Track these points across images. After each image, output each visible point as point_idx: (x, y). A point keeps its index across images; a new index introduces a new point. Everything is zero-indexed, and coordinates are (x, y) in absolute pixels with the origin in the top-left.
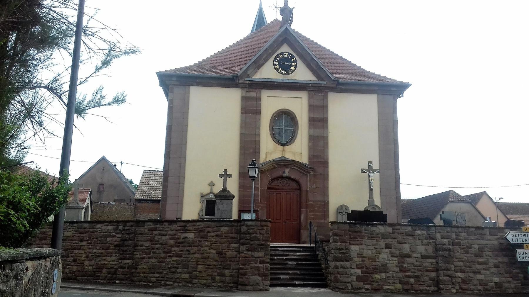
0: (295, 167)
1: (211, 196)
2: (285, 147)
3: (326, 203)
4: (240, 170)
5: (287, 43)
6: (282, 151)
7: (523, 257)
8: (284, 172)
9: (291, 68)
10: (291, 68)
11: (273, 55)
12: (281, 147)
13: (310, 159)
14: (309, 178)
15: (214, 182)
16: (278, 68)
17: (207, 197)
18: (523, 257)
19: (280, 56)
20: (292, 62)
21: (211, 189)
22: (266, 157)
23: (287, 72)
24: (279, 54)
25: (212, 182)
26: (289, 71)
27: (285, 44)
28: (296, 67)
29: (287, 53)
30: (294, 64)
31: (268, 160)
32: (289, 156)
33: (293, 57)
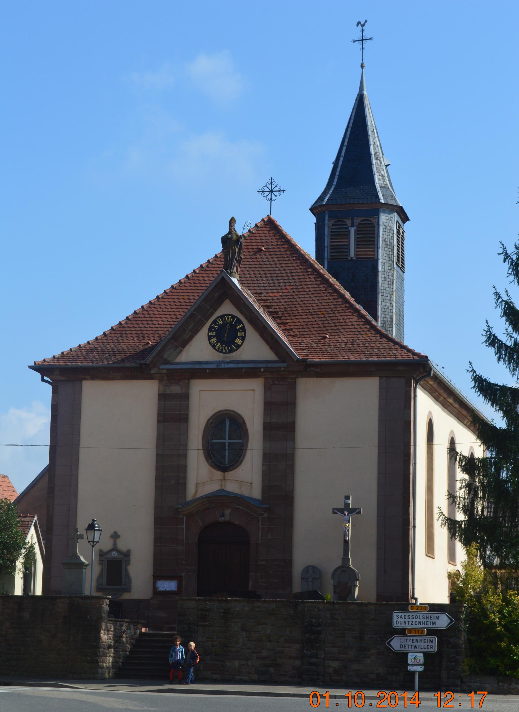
0: (239, 507)
1: (114, 554)
2: (226, 473)
3: (288, 563)
4: (155, 514)
5: (229, 300)
6: (222, 480)
7: (401, 616)
8: (223, 515)
9: (236, 341)
10: (236, 341)
11: (324, 252)
12: (219, 474)
13: (263, 492)
14: (260, 523)
15: (119, 533)
16: (215, 343)
17: (108, 556)
18: (401, 616)
19: (218, 323)
20: (238, 331)
21: (115, 544)
22: (196, 491)
23: (229, 348)
24: (218, 318)
25: (115, 533)
26: (233, 346)
27: (227, 301)
28: (243, 338)
29: (230, 317)
30: (240, 334)
31: (198, 496)
32: (231, 487)
33: (239, 322)
